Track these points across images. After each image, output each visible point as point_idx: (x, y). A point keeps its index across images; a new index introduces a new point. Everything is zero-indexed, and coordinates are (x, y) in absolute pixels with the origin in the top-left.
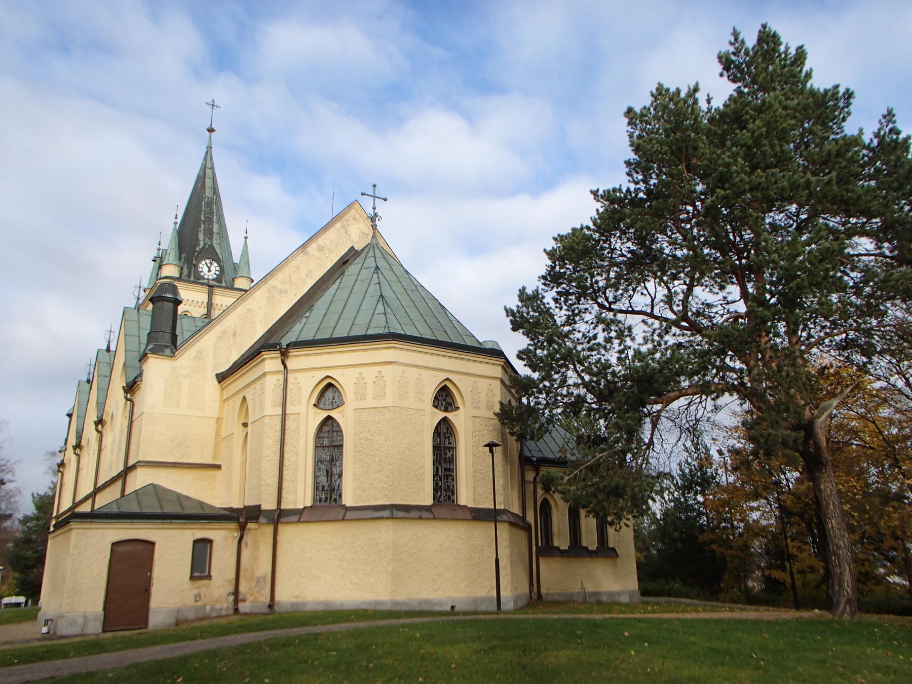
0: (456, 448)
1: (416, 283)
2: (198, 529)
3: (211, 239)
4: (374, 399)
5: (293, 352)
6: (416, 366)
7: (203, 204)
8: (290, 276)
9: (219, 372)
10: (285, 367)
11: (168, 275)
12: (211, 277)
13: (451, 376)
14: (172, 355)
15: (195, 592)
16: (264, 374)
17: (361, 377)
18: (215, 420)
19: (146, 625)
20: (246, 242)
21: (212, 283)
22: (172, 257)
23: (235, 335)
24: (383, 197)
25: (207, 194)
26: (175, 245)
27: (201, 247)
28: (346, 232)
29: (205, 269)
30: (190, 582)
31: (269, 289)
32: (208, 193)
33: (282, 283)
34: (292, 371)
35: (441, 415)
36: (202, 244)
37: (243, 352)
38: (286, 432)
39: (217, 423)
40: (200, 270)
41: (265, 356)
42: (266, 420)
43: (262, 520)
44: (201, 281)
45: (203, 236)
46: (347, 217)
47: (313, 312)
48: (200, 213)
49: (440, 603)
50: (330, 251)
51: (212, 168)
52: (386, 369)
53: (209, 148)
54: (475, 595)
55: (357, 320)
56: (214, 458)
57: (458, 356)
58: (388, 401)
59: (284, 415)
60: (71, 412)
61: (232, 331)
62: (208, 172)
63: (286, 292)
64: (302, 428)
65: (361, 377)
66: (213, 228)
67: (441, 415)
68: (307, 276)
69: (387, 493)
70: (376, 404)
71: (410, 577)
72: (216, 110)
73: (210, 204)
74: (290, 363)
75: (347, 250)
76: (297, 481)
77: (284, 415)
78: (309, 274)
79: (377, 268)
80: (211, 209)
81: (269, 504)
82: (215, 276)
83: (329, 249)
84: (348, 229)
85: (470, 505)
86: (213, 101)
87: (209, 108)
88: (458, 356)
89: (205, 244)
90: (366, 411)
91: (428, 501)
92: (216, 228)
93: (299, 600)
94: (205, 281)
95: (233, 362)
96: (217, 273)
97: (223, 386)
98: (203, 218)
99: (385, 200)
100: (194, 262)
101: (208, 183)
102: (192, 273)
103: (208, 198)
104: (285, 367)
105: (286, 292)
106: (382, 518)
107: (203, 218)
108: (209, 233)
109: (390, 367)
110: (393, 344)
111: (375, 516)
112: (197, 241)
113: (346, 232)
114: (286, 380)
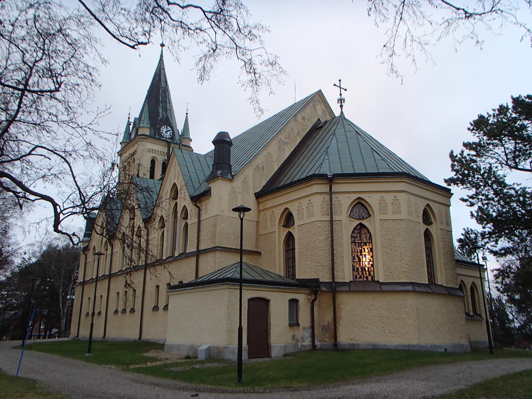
4: (393, 214)
9: (256, 192)
13: (431, 204)
17: (382, 200)
18: (255, 223)
19: (268, 355)
20: (187, 117)
21: (169, 140)
24: (345, 88)
27: (161, 117)
29: (165, 130)
33: (286, 138)
34: (334, 192)
35: (287, 231)
36: (161, 115)
37: (268, 180)
40: (162, 132)
44: (162, 138)
48: (159, 97)
49: (440, 347)
52: (400, 196)
53: (162, 56)
56: (256, 247)
57: (432, 190)
58: (403, 216)
59: (332, 221)
61: (261, 166)
63: (287, 144)
65: (382, 200)
66: (167, 106)
67: (426, 227)
70: (394, 217)
76: (343, 264)
77: (332, 221)
78: (298, 134)
81: (325, 278)
82: (170, 136)
84: (316, 107)
85: (445, 285)
88: (432, 190)
89: (163, 116)
90: (388, 221)
93: (354, 342)
94: (164, 139)
95: (263, 186)
96: (171, 134)
98: (161, 100)
100: (158, 127)
102: (157, 134)
105: (287, 144)
107: (161, 100)
108: (165, 109)
109: (403, 194)
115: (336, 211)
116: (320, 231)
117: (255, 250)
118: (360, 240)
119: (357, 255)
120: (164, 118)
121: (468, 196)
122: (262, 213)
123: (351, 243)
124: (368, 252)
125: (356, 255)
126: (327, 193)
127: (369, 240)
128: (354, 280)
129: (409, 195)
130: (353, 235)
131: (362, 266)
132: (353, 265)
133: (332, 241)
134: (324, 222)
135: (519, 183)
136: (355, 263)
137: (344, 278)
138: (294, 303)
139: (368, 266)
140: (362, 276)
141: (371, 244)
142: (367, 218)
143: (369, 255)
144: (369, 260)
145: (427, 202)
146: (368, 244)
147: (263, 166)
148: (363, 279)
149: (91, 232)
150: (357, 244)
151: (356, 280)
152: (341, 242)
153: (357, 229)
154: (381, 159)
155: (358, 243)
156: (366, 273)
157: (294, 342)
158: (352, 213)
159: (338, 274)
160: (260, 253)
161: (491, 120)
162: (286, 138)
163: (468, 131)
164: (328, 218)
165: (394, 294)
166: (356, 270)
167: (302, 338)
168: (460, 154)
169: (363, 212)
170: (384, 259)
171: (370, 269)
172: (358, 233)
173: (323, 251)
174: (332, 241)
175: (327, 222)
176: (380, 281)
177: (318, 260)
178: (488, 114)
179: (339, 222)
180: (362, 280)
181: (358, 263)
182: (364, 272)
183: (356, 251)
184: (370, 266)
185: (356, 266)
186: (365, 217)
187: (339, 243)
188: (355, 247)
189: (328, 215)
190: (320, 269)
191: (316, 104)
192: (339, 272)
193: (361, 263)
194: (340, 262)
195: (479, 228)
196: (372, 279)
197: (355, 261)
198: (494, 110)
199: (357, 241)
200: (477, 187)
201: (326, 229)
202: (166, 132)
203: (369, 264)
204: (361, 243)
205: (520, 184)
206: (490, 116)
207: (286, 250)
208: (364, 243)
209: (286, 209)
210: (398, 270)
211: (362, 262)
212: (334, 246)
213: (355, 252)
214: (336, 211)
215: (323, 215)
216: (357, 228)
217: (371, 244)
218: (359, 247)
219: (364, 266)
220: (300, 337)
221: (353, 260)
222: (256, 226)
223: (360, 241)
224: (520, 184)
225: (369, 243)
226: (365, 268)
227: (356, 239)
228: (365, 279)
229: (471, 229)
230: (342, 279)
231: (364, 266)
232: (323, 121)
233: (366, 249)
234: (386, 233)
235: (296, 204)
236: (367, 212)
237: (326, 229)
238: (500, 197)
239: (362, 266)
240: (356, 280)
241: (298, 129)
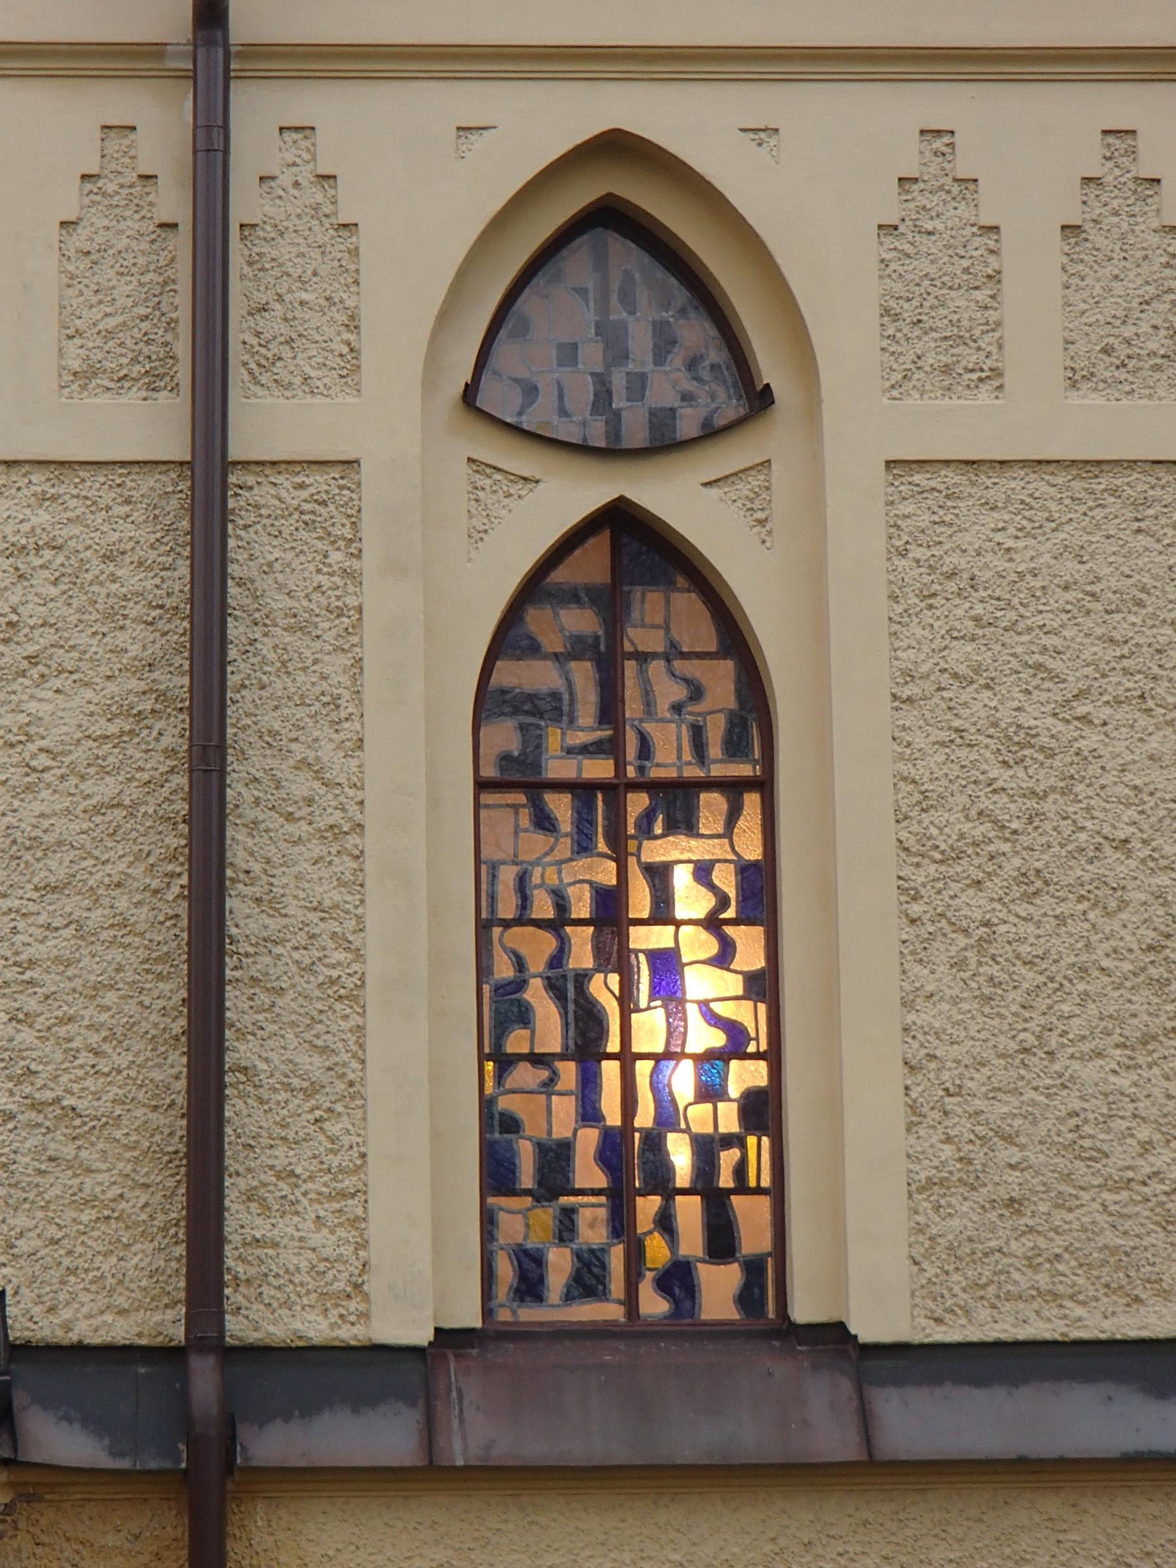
34: (255, 51)
76: (355, 1091)
115: (272, 325)
118: (612, 748)
119: (557, 960)
123: (482, 785)
124: (712, 923)
125: (537, 964)
126: (154, 51)
127: (735, 747)
128: (504, 1315)
130: (509, 674)
131: (613, 1118)
132: (486, 1104)
134: (95, 485)
136: (525, 1075)
139: (699, 1117)
140: (616, 1259)
141: (752, 801)
142: (711, 433)
143: (723, 958)
144: (717, 1039)
146: (712, 806)
148: (631, 1301)
150: (561, 806)
151: (529, 1314)
152: (339, 767)
153: (571, 596)
155: (582, 790)
156: (665, 1223)
158: (506, 355)
159: (286, 1227)
161: (297, 1413)
165: (1051, 1504)
166: (527, 1178)
169: (664, 344)
170: (925, 1016)
171: (728, 1159)
172: (578, 648)
173: (72, 904)
175: (149, 482)
176: (866, 1329)
179: (318, 481)
180: (610, 1311)
181: (569, 1072)
182: (648, 1206)
183: (543, 908)
184: (729, 1119)
185: (533, 1128)
186: (687, 426)
187: (301, 785)
188: (538, 842)
189: (154, 382)
192: (290, 1206)
193: (610, 1070)
194: (313, 1064)
196: (750, 1298)
197: (517, 1041)
199: (557, 768)
201: (133, 580)
203: (710, 1093)
204: (615, 790)
208: (653, 787)
210: (1112, 1167)
211: (627, 1058)
212: (236, 834)
213: (522, 920)
214: (272, 325)
215: (86, 375)
216: (560, 576)
217: (752, 801)
218: (583, 847)
219: (645, 1117)
221: (502, 1027)
223: (600, 769)
225: (734, 789)
226: (654, 1142)
227: (554, 739)
228: (653, 1304)
230: (327, 1299)
231: (645, 1117)
233: (682, 877)
234: (960, 655)
236: (716, 355)
237: (133, 580)
239: (613, 1118)
240: (529, 1314)
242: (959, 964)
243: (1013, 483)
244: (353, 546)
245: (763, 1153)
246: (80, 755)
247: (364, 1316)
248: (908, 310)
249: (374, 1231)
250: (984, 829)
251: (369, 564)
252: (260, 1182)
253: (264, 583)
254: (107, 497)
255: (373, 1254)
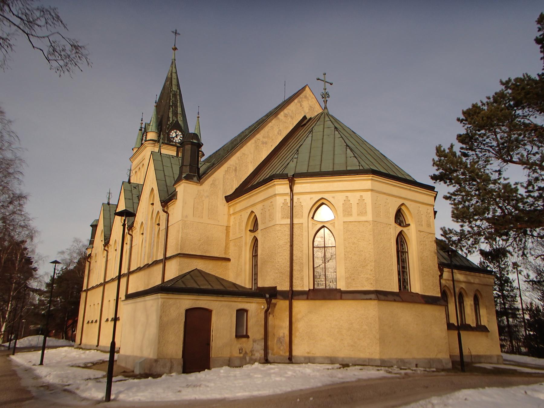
0: (408, 252)
1: (362, 140)
2: (240, 302)
3: (177, 117)
5: (297, 180)
6: (384, 193)
7: (171, 95)
8: (268, 133)
10: (292, 190)
11: (151, 139)
12: (177, 141)
14: (198, 182)
15: (239, 346)
16: (275, 195)
17: (347, 200)
18: (225, 228)
22: (153, 127)
23: (236, 170)
25: (173, 89)
26: (154, 120)
27: (171, 122)
28: (301, 106)
29: (174, 135)
30: (236, 339)
31: (256, 140)
32: (174, 88)
33: (264, 137)
36: (171, 119)
37: (241, 182)
38: (294, 236)
39: (226, 230)
41: (275, 183)
42: (278, 228)
43: (279, 297)
44: (172, 143)
45: (172, 115)
46: (301, 96)
47: (299, 155)
50: (292, 118)
51: (176, 73)
54: (428, 357)
55: (297, 168)
56: (225, 253)
57: (409, 188)
59: (292, 225)
60: (95, 224)
61: (234, 168)
62: (174, 75)
63: (266, 143)
64: (305, 234)
65: (347, 200)
67: (399, 229)
68: (278, 133)
69: (372, 282)
71: (390, 342)
72: (178, 36)
73: (175, 95)
74: (297, 188)
75: (301, 118)
77: (292, 225)
78: (280, 133)
79: (336, 128)
80: (176, 98)
81: (284, 286)
82: (180, 141)
83: (291, 117)
85: (420, 293)
86: (176, 31)
87: (174, 35)
88: (409, 188)
89: (173, 120)
91: (396, 290)
92: (179, 110)
94: (174, 144)
96: (181, 139)
97: (230, 205)
99: (331, 84)
101: (174, 82)
103: (174, 91)
104: (292, 190)
105: (266, 143)
106: (371, 299)
110: (370, 177)
111: (365, 298)
112: (169, 118)
113: (301, 106)
114: (292, 200)
115: (297, 213)
116: (279, 235)
117: (224, 256)
120: (174, 122)
121: (449, 193)
122: (232, 217)
129: (378, 194)
133: (292, 246)
134: (284, 226)
135: (506, 177)
137: (303, 286)
138: (241, 313)
145: (401, 202)
147: (236, 168)
149: (92, 240)
154: (353, 155)
157: (242, 355)
160: (229, 260)
162: (264, 137)
163: (457, 122)
164: (288, 221)
167: (252, 351)
168: (449, 149)
174: (292, 246)
177: (277, 266)
178: (482, 102)
190: (278, 276)
191: (302, 100)
195: (456, 227)
198: (489, 98)
200: (458, 182)
202: (176, 136)
205: (508, 179)
206: (483, 104)
207: (253, 256)
209: (252, 212)
220: (250, 350)
222: (226, 231)
224: (508, 179)
229: (449, 229)
232: (308, 117)
234: (349, 236)
235: (259, 206)
238: (480, 193)
241: (279, 128)
242: (349, 261)
243: (353, 223)
244: (302, 230)
245: (249, 148)
246: (283, 246)
247: (303, 288)
248: (345, 210)
249: (304, 281)
250: (351, 250)
251: (304, 231)
252: (518, 134)
253: (296, 233)
254: (284, 226)
255: (304, 283)
